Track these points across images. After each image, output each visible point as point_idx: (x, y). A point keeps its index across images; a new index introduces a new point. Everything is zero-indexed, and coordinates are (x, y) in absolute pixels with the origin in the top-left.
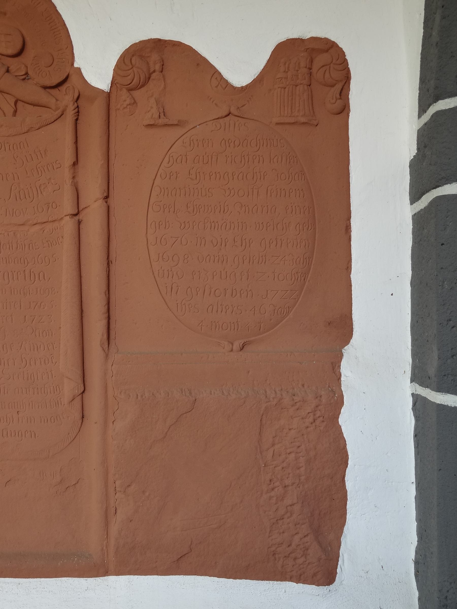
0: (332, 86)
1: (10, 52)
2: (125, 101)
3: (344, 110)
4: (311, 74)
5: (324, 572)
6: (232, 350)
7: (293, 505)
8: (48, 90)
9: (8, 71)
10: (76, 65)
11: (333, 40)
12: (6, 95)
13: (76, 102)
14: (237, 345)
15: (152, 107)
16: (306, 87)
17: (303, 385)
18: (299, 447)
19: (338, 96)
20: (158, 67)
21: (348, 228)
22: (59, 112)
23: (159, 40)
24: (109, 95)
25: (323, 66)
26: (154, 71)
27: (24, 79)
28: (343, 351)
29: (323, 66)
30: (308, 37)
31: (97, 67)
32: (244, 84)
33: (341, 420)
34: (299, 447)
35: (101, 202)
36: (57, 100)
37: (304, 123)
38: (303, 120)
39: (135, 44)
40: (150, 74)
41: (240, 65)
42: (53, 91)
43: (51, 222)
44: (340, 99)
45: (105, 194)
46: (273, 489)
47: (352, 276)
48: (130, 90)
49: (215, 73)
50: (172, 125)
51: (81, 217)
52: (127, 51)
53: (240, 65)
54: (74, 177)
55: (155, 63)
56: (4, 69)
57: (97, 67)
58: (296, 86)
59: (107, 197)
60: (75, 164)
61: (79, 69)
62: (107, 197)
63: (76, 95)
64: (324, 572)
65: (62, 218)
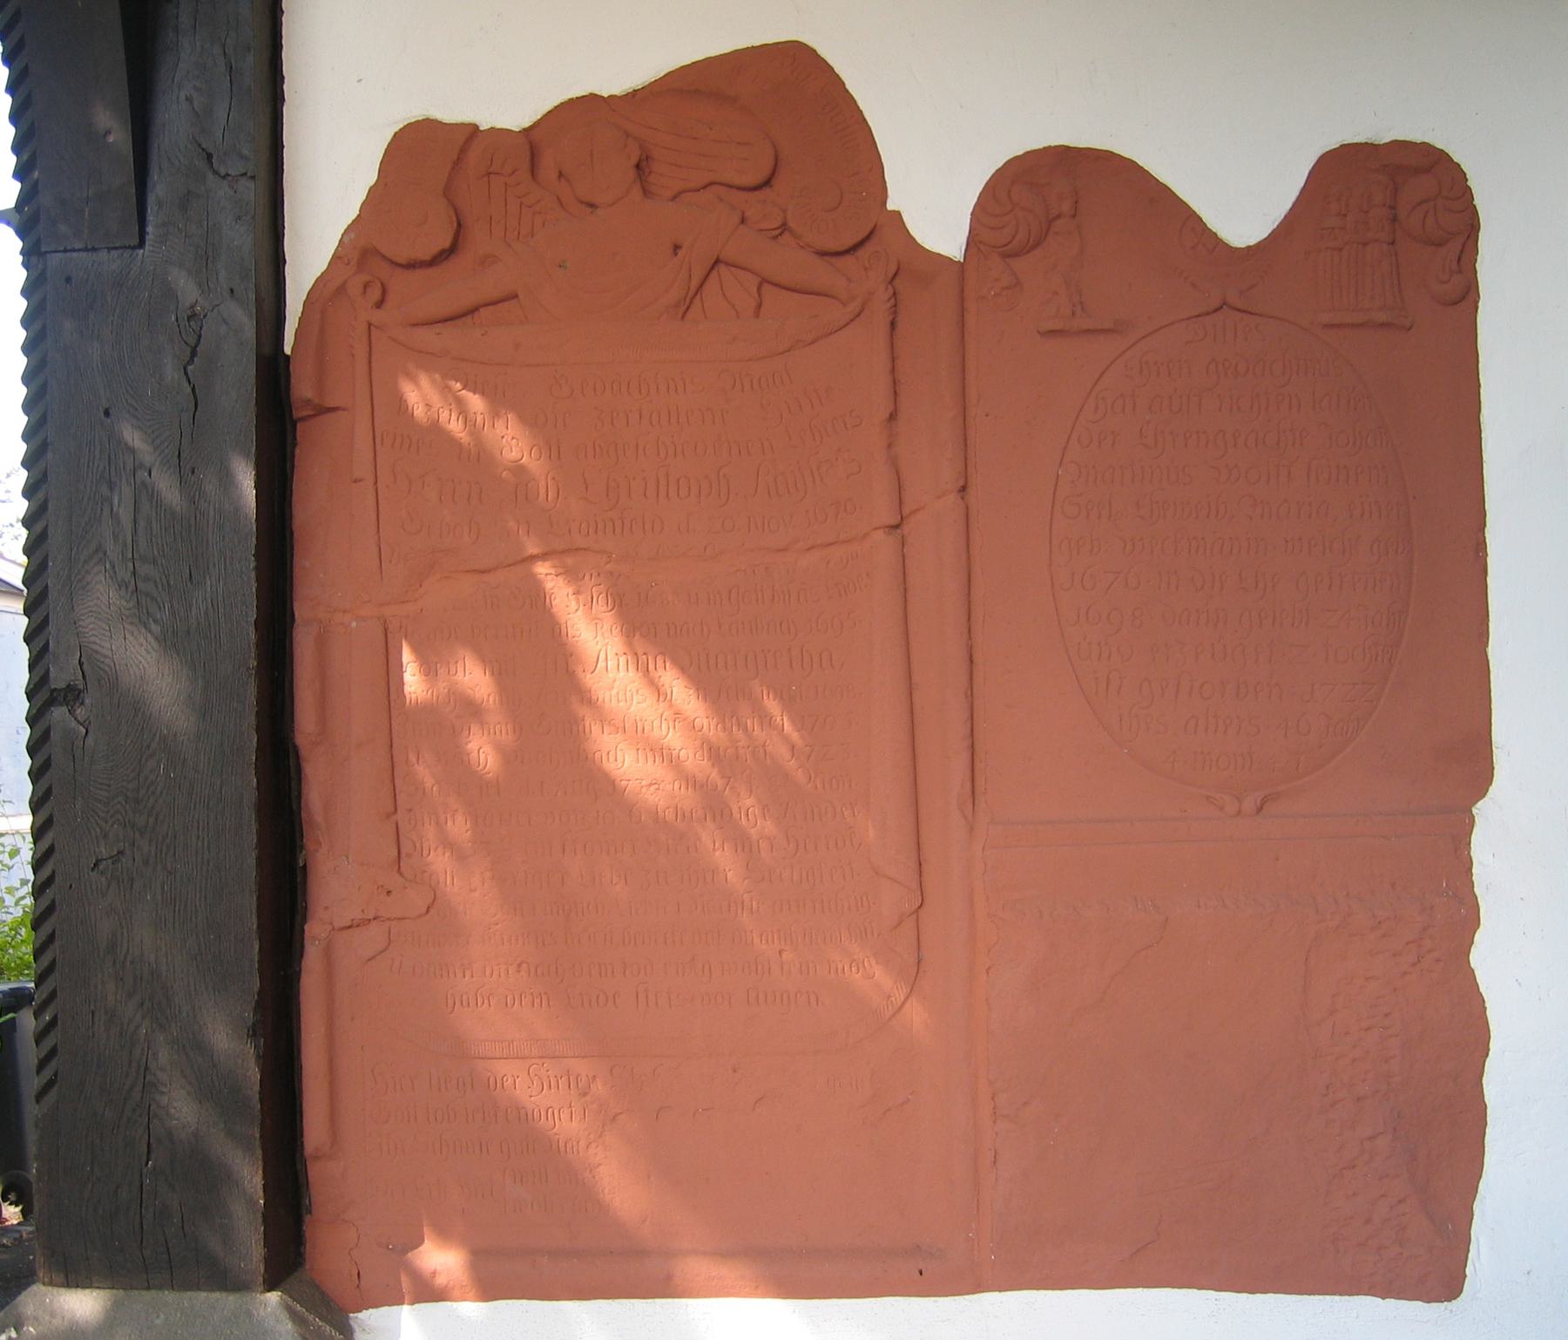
0: (1440, 244)
1: (749, 179)
2: (997, 280)
3: (1467, 295)
4: (1394, 219)
5: (1436, 1273)
6: (1239, 813)
7: (1370, 1138)
8: (833, 260)
9: (743, 221)
10: (890, 206)
11: (1439, 146)
12: (741, 273)
13: (891, 282)
14: (1249, 804)
15: (1056, 293)
16: (1385, 247)
17: (1393, 885)
18: (1386, 1015)
19: (1454, 266)
20: (1066, 207)
21: (1481, 546)
22: (854, 307)
23: (1067, 149)
24: (962, 266)
25: (1419, 204)
26: (1059, 216)
27: (775, 238)
28: (1474, 811)
29: (1419, 204)
30: (1387, 140)
31: (934, 205)
32: (1252, 242)
33: (1476, 958)
34: (1386, 1015)
35: (952, 498)
36: (849, 280)
37: (1383, 325)
38: (1383, 317)
39: (1016, 158)
40: (1050, 222)
41: (1242, 195)
42: (849, 261)
43: (844, 542)
44: (1460, 272)
45: (961, 483)
46: (1332, 1105)
47: (1490, 650)
48: (1005, 256)
49: (1190, 219)
50: (1102, 331)
51: (906, 528)
52: (999, 174)
53: (1242, 195)
54: (889, 446)
55: (1062, 200)
56: (736, 219)
57: (934, 205)
58: (1365, 244)
59: (963, 489)
60: (892, 417)
61: (897, 214)
62: (963, 489)
63: (893, 269)
64: (1436, 1273)
65: (865, 536)
